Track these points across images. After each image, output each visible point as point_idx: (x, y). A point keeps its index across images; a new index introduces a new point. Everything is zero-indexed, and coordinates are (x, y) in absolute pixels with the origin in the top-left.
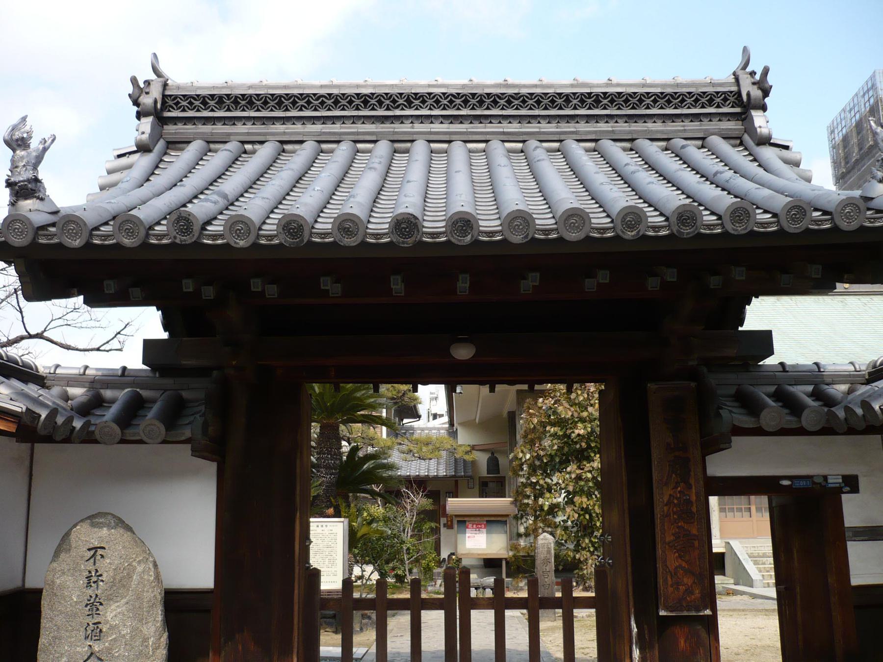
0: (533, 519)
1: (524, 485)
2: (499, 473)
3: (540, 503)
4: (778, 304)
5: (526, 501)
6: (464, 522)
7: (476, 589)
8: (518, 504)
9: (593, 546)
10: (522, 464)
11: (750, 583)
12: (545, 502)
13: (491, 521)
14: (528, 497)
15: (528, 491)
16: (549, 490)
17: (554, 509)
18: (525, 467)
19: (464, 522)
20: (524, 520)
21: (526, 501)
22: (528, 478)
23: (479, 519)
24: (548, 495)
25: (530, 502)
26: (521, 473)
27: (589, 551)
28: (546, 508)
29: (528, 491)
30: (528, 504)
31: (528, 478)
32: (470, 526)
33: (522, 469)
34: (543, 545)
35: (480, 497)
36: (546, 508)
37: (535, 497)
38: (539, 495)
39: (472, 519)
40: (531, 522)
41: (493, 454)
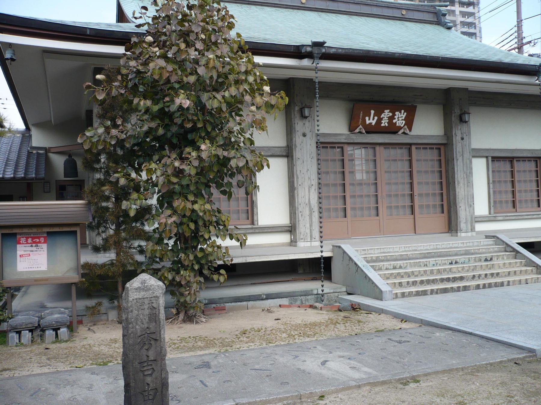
0: (113, 227)
1: (102, 183)
2: (77, 176)
3: (123, 207)
4: (351, 19)
5: (104, 204)
6: (15, 235)
7: (31, 331)
8: (93, 208)
9: (198, 262)
10: (99, 154)
11: (379, 295)
12: (132, 206)
13: (52, 231)
14: (107, 199)
15: (107, 190)
16: (137, 189)
17: (144, 213)
18: (103, 158)
19: (15, 235)
20: (102, 229)
21: (104, 204)
22: (107, 174)
23: (34, 230)
24: (135, 195)
25: (110, 205)
26: (97, 166)
27: (193, 269)
28: (132, 214)
29: (107, 190)
30: (107, 208)
31: (107, 174)
32: (23, 240)
33: (99, 161)
34: (140, 302)
35: (57, 199)
36: (132, 214)
37: (117, 199)
38: (122, 194)
39: (25, 230)
40: (112, 232)
41: (70, 156)
